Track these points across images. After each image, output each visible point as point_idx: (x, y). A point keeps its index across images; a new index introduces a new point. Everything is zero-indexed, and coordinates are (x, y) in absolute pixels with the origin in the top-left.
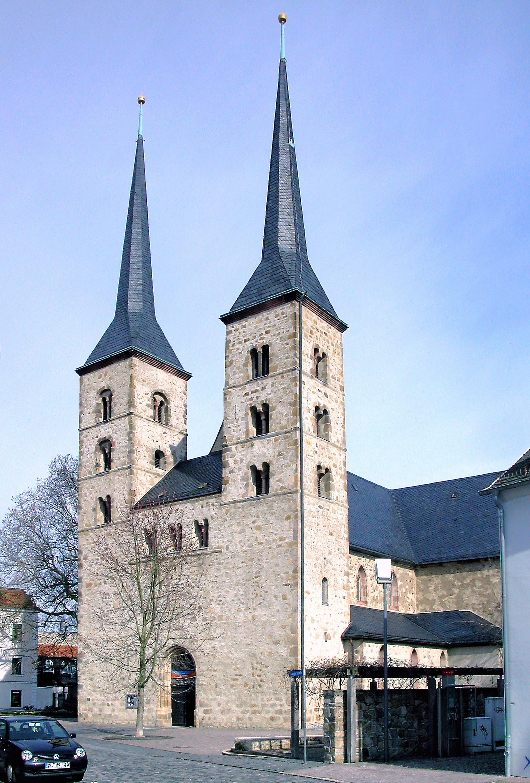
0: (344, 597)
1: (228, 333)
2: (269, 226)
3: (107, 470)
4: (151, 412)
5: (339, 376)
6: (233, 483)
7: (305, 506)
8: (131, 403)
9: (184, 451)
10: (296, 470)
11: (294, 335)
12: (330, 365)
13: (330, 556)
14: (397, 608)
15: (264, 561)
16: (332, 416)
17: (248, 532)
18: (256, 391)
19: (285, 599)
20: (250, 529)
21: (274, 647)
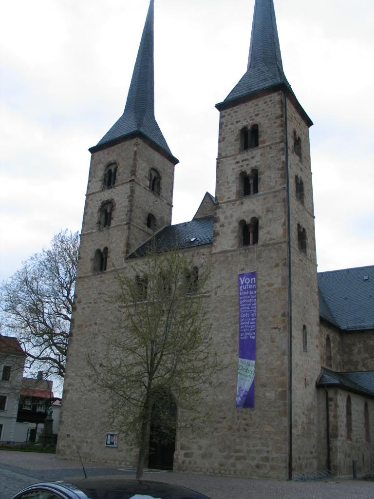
1: (221, 117)
8: (133, 173)
11: (282, 116)
14: (331, 366)
18: (246, 160)
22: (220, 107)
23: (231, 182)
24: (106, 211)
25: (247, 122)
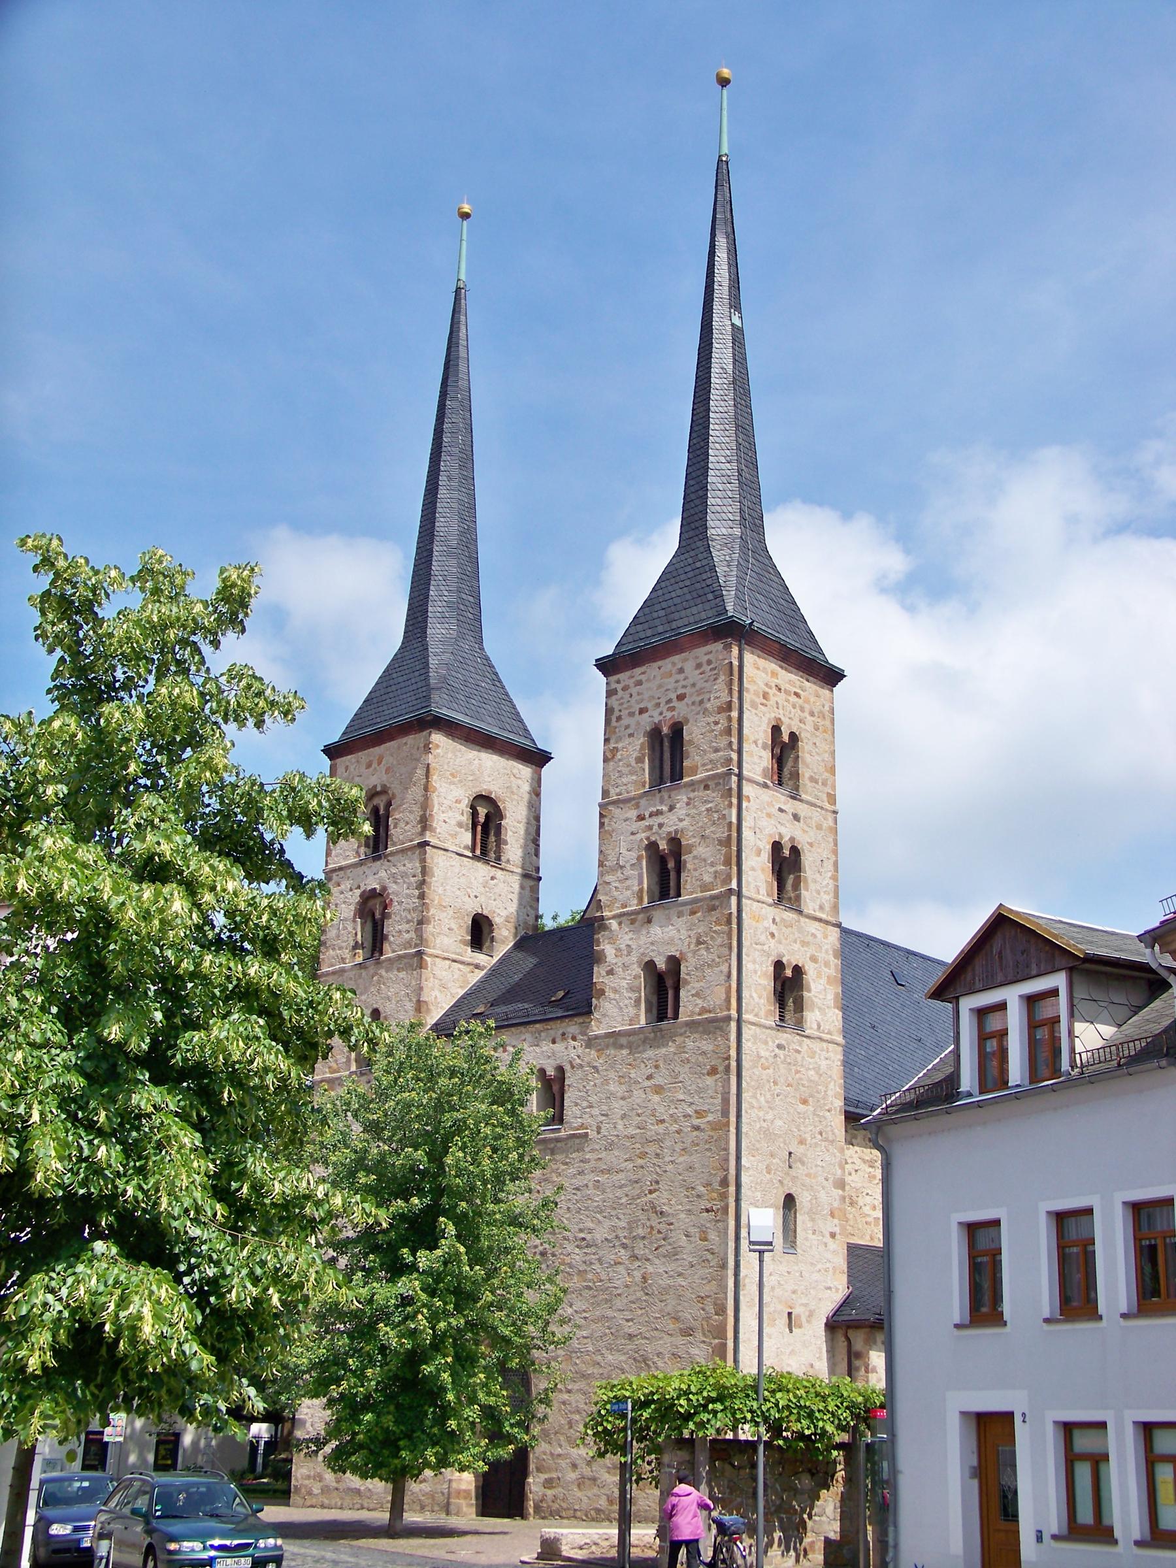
0: (833, 1235)
1: (610, 693)
2: (691, 482)
3: (377, 954)
4: (467, 838)
5: (827, 775)
6: (612, 996)
7: (747, 1045)
8: (425, 823)
9: (532, 913)
10: (729, 976)
12: (807, 756)
13: (802, 1149)
15: (667, 1159)
16: (808, 860)
17: (638, 1095)
19: (705, 1239)
20: (641, 1091)
21: (680, 1340)
22: (607, 666)
23: (628, 866)
24: (373, 915)
25: (661, 714)
